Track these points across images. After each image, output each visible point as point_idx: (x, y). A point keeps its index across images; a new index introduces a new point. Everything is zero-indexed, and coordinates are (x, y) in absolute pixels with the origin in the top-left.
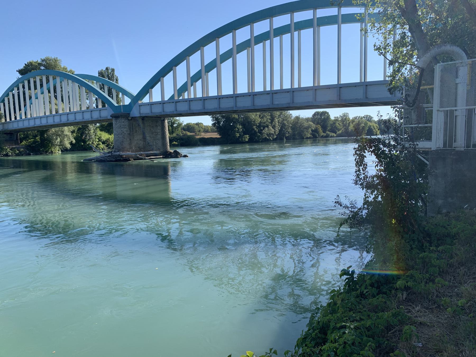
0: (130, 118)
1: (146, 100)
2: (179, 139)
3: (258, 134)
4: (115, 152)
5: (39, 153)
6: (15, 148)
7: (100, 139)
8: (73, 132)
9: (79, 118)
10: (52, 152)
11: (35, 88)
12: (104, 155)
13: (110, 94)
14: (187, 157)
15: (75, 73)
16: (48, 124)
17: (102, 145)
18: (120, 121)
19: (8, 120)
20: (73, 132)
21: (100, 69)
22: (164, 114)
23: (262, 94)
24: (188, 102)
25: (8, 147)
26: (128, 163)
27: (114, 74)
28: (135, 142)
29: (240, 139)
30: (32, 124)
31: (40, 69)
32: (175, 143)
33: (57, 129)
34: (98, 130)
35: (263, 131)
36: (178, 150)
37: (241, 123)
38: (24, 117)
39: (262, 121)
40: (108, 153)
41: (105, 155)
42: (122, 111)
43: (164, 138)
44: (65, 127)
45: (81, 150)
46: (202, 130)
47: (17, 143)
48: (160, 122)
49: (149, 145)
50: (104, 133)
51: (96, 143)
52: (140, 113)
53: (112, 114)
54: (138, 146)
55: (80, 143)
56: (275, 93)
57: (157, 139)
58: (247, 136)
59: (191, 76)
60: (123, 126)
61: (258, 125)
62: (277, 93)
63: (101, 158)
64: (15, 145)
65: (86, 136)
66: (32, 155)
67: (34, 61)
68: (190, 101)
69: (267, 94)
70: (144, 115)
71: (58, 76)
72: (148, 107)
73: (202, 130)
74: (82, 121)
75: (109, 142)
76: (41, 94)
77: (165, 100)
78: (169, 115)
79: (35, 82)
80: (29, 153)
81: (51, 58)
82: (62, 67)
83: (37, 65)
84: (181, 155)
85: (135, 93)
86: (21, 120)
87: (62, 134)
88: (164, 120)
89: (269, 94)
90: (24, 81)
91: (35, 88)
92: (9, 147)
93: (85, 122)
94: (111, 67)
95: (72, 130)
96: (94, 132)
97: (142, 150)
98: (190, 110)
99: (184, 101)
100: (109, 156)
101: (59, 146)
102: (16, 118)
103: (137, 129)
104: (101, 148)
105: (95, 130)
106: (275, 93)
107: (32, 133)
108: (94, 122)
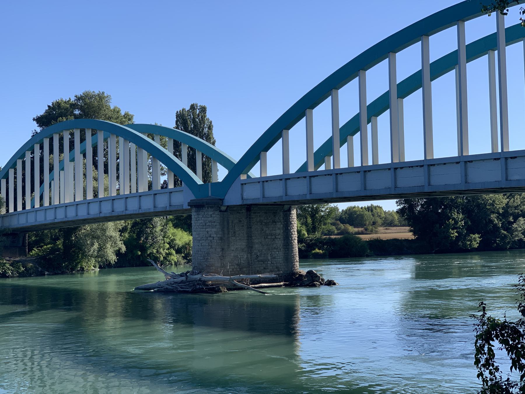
0: (223, 208)
1: (255, 172)
2: (326, 243)
3: (503, 231)
4: (193, 273)
5: (60, 272)
6: (18, 262)
7: (172, 244)
8: (122, 231)
9: (133, 207)
10: (82, 269)
11: (61, 151)
12: (172, 280)
13: (192, 165)
14: (334, 284)
15: (137, 121)
16: (77, 218)
17: (175, 255)
18: (206, 213)
19: (11, 210)
20: (122, 231)
21: (179, 109)
22: (288, 200)
23: (483, 160)
24: (334, 176)
25: (6, 260)
26: (215, 296)
27: (205, 117)
28: (232, 255)
29: (460, 243)
30: (50, 217)
31: (72, 114)
32: (318, 251)
33: (95, 226)
34: (170, 224)
35: (515, 225)
36: (314, 269)
37: (462, 209)
38: (37, 205)
39: (510, 204)
40: (181, 275)
41: (176, 280)
42: (210, 194)
43: (289, 245)
44: (109, 223)
45: (137, 266)
46: (380, 221)
47: (22, 253)
48: (281, 214)
49: (258, 261)
50: (181, 232)
51: (163, 252)
52: (242, 198)
53: (191, 201)
54: (237, 262)
55: (135, 251)
56: (511, 158)
57: (275, 248)
58: (477, 235)
59: (398, 82)
60: (210, 224)
61: (501, 211)
62: (516, 157)
63: (167, 285)
64: (20, 255)
65: (147, 238)
66: (47, 274)
67: (64, 100)
68: (338, 173)
69: (495, 159)
70: (249, 202)
71: (101, 130)
72: (258, 186)
73: (380, 221)
74: (137, 212)
75: (189, 250)
76: (70, 161)
77: (290, 173)
78: (298, 201)
79: (61, 139)
80: (41, 271)
81: (93, 94)
82: (112, 108)
83: (68, 108)
84: (323, 280)
85: (236, 157)
86: (33, 209)
87: (104, 235)
88: (289, 210)
89: (499, 159)
90: (43, 139)
91: (61, 151)
92: (8, 260)
93: (143, 214)
94: (200, 103)
95: (121, 227)
96: (162, 230)
97: (245, 269)
98: (337, 191)
99: (328, 173)
100: (182, 282)
101: (96, 257)
102: (24, 207)
103: (237, 229)
104: (173, 262)
105: (163, 226)
106: (511, 158)
107: (51, 233)
108: (158, 214)
